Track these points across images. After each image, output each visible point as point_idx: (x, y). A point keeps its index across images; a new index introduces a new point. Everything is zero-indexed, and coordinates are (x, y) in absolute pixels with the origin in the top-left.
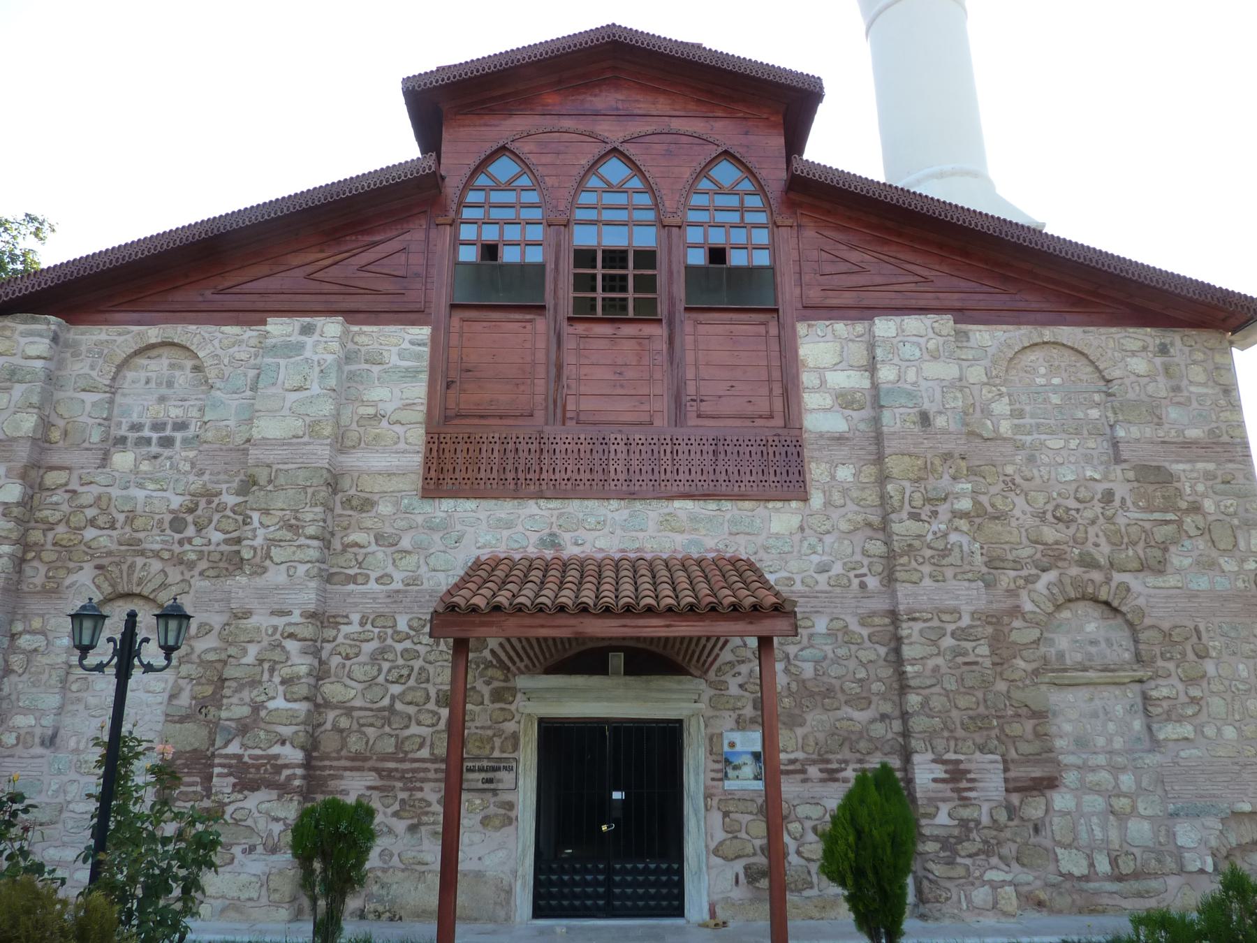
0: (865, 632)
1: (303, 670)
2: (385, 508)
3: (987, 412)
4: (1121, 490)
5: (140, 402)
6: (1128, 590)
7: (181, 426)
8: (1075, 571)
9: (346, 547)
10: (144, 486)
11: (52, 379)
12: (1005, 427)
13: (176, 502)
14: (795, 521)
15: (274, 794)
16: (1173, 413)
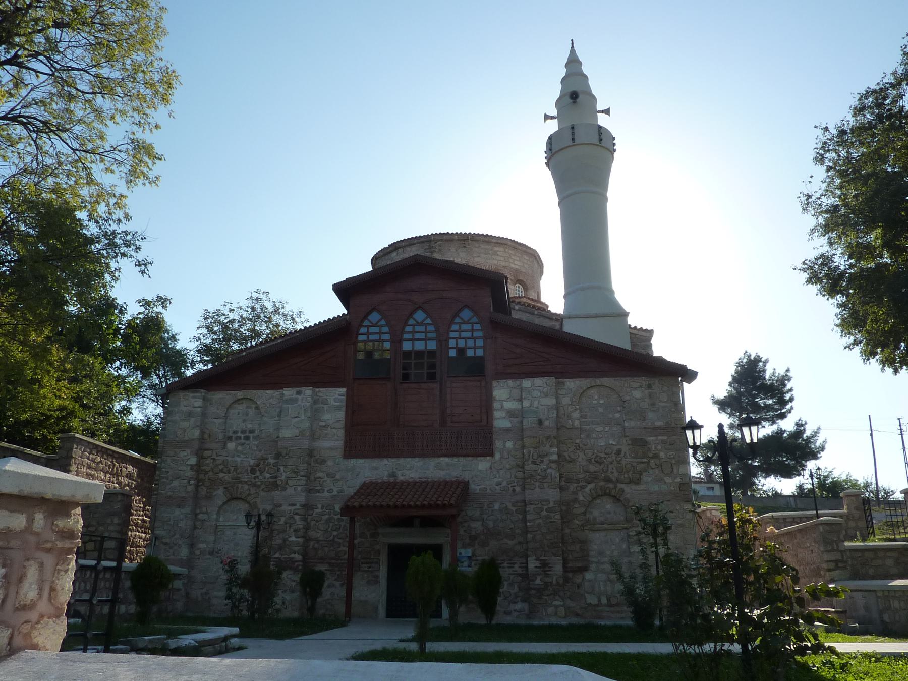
0: (514, 509)
1: (301, 526)
2: (330, 463)
3: (569, 417)
4: (625, 449)
5: (236, 423)
6: (623, 491)
7: (252, 432)
8: (602, 484)
9: (315, 479)
10: (240, 456)
11: (204, 415)
12: (577, 423)
13: (252, 462)
14: (488, 465)
15: (291, 572)
16: (650, 415)
